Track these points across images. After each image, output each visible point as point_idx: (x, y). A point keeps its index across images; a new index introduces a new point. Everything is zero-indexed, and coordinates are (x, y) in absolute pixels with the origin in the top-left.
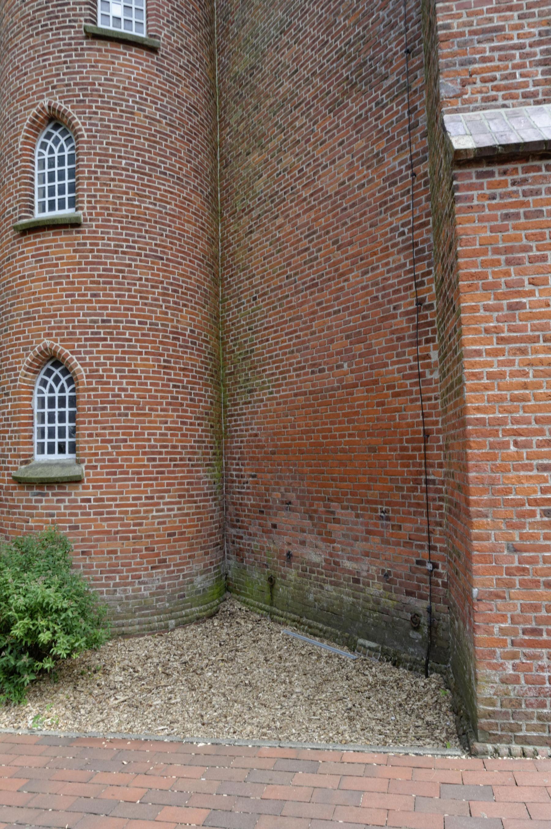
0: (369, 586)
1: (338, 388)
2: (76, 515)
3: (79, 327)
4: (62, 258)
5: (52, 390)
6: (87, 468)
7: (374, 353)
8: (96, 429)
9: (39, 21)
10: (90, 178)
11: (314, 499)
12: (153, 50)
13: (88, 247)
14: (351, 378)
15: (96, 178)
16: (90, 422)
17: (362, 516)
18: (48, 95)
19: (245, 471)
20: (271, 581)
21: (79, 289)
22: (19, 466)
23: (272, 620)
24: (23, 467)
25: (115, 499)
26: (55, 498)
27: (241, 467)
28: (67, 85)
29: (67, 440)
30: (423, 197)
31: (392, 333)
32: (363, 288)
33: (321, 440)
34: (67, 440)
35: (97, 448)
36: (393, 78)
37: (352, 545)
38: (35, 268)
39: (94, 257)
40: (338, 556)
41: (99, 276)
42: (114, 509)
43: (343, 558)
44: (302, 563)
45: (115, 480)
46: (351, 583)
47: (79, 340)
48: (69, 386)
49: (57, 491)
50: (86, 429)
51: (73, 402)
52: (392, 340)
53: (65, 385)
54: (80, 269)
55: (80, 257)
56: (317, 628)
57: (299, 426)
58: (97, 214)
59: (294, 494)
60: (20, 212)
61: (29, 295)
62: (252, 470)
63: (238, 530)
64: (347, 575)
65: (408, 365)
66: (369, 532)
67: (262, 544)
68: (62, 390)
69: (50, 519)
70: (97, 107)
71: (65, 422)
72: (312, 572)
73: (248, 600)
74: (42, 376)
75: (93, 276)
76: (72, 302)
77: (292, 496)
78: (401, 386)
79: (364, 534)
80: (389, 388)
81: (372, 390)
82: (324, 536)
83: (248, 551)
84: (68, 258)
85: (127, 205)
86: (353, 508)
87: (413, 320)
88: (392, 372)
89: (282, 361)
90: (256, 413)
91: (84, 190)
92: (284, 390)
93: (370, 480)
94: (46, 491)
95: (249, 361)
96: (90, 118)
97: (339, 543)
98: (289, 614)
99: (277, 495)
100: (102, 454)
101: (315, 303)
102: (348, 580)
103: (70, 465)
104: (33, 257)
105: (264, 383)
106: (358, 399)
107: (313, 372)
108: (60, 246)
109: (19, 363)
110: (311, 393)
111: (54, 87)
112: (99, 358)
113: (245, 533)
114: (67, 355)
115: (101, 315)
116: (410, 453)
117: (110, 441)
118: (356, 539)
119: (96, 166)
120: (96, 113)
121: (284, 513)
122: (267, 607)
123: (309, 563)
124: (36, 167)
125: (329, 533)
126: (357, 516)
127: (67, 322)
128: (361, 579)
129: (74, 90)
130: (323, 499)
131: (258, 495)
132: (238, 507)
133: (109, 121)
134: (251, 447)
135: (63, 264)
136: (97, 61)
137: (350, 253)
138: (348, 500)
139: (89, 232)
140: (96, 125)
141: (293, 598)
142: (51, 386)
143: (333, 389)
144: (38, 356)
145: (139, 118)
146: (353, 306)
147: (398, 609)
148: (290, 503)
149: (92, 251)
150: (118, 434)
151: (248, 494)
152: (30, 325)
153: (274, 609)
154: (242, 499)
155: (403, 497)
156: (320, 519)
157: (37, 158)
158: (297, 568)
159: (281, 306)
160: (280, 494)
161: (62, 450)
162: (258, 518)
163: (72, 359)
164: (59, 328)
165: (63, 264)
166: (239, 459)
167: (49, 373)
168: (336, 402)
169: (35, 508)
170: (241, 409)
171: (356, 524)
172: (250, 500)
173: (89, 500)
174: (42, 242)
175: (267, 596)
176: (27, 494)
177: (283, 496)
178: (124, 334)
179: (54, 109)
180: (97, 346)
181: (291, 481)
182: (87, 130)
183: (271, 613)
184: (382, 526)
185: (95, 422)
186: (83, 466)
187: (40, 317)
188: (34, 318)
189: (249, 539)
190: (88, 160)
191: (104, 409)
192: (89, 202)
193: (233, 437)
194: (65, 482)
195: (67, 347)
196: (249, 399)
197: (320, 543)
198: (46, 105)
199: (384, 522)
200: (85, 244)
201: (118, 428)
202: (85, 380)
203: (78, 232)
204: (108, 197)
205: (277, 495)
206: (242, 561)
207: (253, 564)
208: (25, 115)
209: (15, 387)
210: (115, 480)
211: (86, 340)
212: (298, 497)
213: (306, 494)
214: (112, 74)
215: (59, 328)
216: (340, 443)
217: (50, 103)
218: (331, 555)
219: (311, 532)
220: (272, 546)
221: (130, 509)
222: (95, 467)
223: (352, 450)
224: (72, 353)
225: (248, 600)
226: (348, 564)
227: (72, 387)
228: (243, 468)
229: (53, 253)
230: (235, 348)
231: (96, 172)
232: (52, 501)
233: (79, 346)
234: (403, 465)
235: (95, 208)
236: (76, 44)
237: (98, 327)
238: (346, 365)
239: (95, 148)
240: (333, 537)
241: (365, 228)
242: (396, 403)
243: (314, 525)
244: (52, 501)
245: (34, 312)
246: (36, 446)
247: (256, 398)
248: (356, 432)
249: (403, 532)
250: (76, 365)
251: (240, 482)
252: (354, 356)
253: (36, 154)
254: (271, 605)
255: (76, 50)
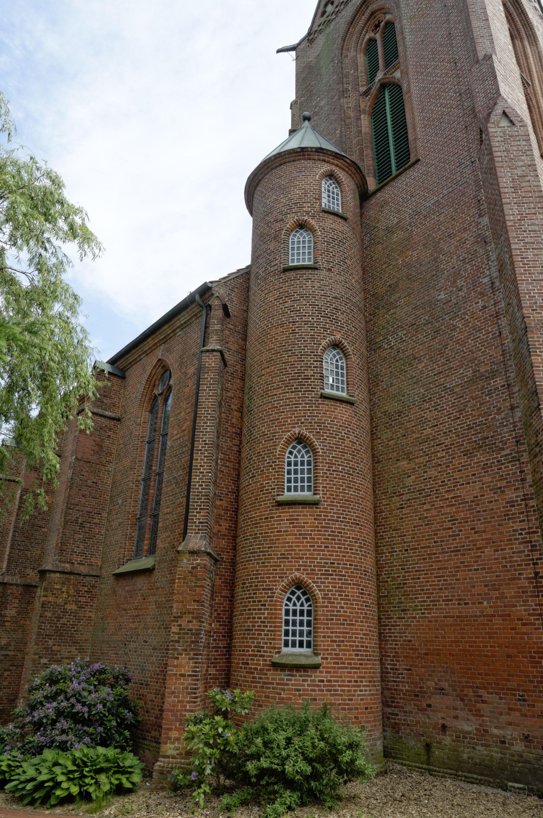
0: (513, 745)
1: (480, 616)
2: (315, 691)
3: (317, 566)
4: (307, 523)
5: (295, 605)
6: (322, 658)
7: (506, 598)
8: (327, 633)
9: (293, 386)
10: (323, 477)
11: (463, 687)
12: (352, 404)
13: (323, 517)
14: (490, 611)
15: (327, 477)
16: (324, 628)
17: (505, 698)
18: (298, 427)
19: (400, 665)
20: (428, 747)
21: (317, 543)
22: (274, 655)
23: (431, 775)
24: (277, 655)
25: (337, 681)
26: (301, 678)
27: (395, 662)
28: (310, 423)
29: (305, 639)
30: (533, 518)
31: (519, 588)
32: (495, 559)
33: (468, 648)
34: (305, 639)
35: (328, 646)
36: (508, 452)
37: (498, 718)
38: (289, 527)
39: (326, 523)
40: (487, 726)
41: (329, 535)
42: (337, 688)
43: (491, 727)
44: (456, 732)
45: (339, 668)
46: (499, 744)
47: (317, 574)
48: (307, 602)
49: (302, 673)
50: (322, 632)
51: (309, 613)
52: (519, 592)
53: (304, 602)
54: (318, 531)
55: (318, 523)
56: (473, 778)
57: (449, 638)
58: (328, 498)
59: (447, 683)
60: (278, 491)
61: (284, 543)
62: (407, 665)
63: (393, 709)
64: (495, 739)
65: (531, 608)
66: (510, 709)
67: (418, 719)
68: (302, 605)
69: (297, 693)
70: (327, 436)
71: (303, 626)
72: (465, 738)
73: (404, 762)
74: (288, 595)
75: (325, 535)
76: (314, 550)
77: (445, 685)
78: (527, 619)
79: (507, 710)
80: (518, 620)
81: (506, 620)
82: (474, 712)
83: (403, 724)
84: (311, 523)
85: (342, 493)
86: (496, 693)
87: (532, 583)
88: (521, 611)
89: (432, 593)
90: (410, 625)
91: (320, 483)
92: (434, 613)
93: (509, 675)
94: (295, 673)
95: (402, 590)
96: (323, 442)
97: (487, 717)
98: (445, 770)
99: (431, 684)
100: (331, 650)
101: (459, 561)
102: (497, 742)
103: (310, 656)
104: (287, 520)
105: (416, 606)
106: (496, 624)
107: (459, 604)
108: (306, 515)
109: (276, 585)
110: (458, 617)
111: (302, 423)
112: (329, 587)
113: (400, 711)
114: (310, 583)
115: (330, 559)
116: (537, 660)
117: (335, 641)
118: (501, 714)
119: (327, 470)
120: (326, 439)
121: (438, 696)
122: (427, 767)
123: (462, 731)
124: (286, 464)
125: (479, 710)
126: (501, 698)
127: (310, 562)
128: (507, 741)
129: (314, 426)
130: (472, 687)
131: (412, 683)
132: (393, 691)
133: (333, 444)
134: (405, 649)
135: (308, 527)
136: (326, 411)
137: (484, 537)
138: (492, 688)
139: (323, 508)
140: (326, 446)
141: (448, 758)
142: (294, 602)
143: (476, 616)
144: (290, 583)
145: (347, 442)
146: (489, 568)
147: (537, 759)
148: (443, 689)
149: (325, 520)
150: (339, 637)
151: (403, 682)
152: (285, 562)
153: (431, 767)
154: (397, 686)
155: (534, 687)
156: (470, 700)
157: (286, 460)
158: (452, 735)
159: (430, 558)
160: (433, 684)
161: (301, 645)
162: (412, 700)
163: (313, 586)
164: (305, 566)
165: (308, 527)
166: (394, 657)
167: (293, 593)
168: (478, 625)
169: (287, 685)
170: (395, 622)
171: (500, 704)
172: (405, 686)
173: (323, 681)
174: (294, 512)
175: (424, 758)
176: (281, 675)
177: (436, 684)
178: (342, 572)
179: (302, 435)
180: (328, 579)
181: (443, 674)
182: (322, 449)
183: (430, 771)
184: (521, 705)
185: (327, 628)
186: (320, 657)
187: (292, 558)
188: (288, 558)
189: (405, 716)
190: (322, 466)
191: (332, 620)
192: (323, 491)
193: (388, 640)
194: (309, 668)
195: (310, 578)
196: (403, 616)
197: (471, 717)
198: (297, 432)
199: (522, 703)
200: (321, 516)
201: (340, 633)
202: (321, 600)
203: (317, 508)
204: (333, 488)
205: (431, 684)
206: (398, 732)
207: (409, 734)
208: (282, 435)
209: (271, 601)
210: (339, 668)
211: (322, 574)
212: (450, 686)
213: (457, 683)
214: (334, 418)
215: (305, 566)
216: (484, 651)
217: (300, 431)
218: (481, 725)
219: (462, 710)
220: (427, 720)
221: (346, 688)
222: (327, 658)
223: (493, 656)
224: (313, 582)
225: (404, 762)
226: (496, 731)
227: (309, 604)
228: (398, 663)
229: (302, 519)
230: (389, 580)
231: (326, 473)
232: (299, 680)
233: (317, 578)
234: (532, 667)
235: (326, 494)
236: (315, 401)
237: (328, 567)
238: (485, 603)
239: (326, 459)
240: (482, 713)
241: (494, 526)
242: (525, 629)
243: (466, 705)
244: (299, 680)
245: (288, 554)
246: (283, 642)
247: (409, 616)
248: (496, 645)
249: (536, 709)
250: (315, 590)
251: (394, 673)
252: (491, 598)
253: (286, 457)
254: (428, 764)
255: (315, 404)
